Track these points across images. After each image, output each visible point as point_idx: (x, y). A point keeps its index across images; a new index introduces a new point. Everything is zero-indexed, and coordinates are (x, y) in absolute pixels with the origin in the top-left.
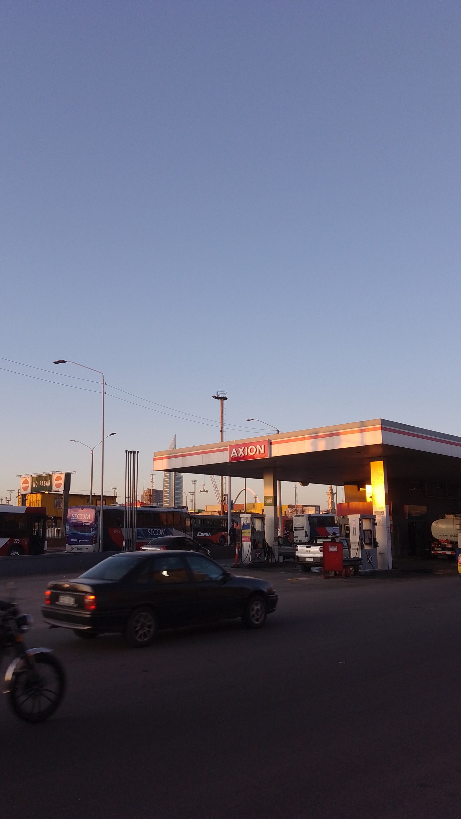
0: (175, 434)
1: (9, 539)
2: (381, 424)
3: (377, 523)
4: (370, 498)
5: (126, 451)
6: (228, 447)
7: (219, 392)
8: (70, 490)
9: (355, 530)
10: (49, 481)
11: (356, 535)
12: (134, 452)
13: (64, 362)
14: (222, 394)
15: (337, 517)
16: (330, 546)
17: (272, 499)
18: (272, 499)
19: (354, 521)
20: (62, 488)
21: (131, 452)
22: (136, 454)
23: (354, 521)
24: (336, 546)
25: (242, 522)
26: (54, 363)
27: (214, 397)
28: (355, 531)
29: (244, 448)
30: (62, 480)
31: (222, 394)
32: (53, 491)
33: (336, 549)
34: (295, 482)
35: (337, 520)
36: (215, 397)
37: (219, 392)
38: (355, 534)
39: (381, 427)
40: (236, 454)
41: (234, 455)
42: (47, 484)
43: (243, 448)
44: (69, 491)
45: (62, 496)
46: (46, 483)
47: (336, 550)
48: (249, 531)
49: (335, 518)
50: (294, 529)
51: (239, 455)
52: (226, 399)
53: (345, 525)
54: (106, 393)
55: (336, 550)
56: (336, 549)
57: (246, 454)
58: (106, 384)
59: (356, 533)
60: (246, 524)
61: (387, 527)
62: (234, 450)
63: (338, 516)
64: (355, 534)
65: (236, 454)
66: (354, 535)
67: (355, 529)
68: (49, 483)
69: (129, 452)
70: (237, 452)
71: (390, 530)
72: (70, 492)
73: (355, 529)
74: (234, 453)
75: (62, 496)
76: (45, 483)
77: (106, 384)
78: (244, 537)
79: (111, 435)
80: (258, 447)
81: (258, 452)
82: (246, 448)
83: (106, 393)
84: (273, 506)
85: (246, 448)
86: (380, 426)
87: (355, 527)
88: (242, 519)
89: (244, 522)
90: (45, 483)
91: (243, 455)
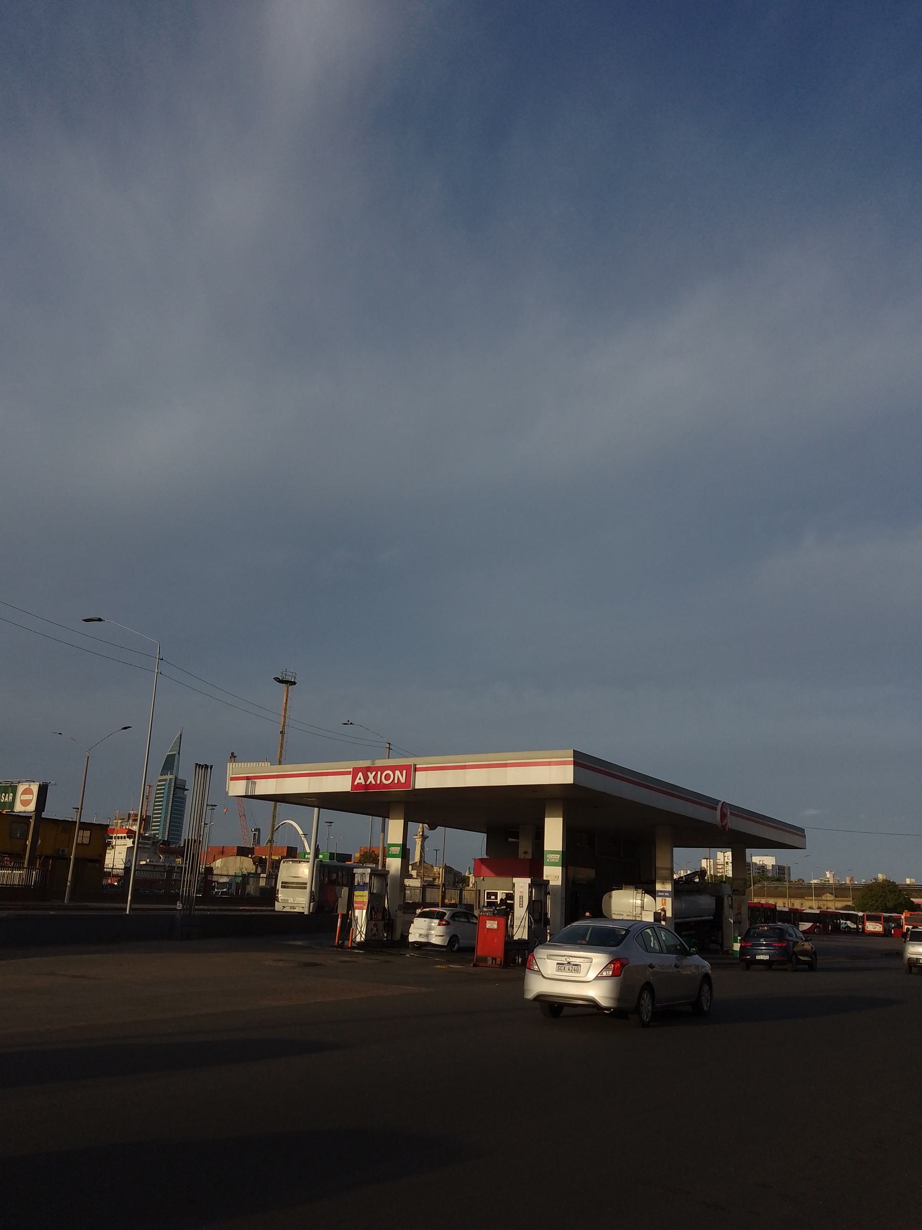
0: (183, 727)
1: (812, 924)
2: (574, 757)
3: (550, 892)
4: (524, 853)
5: (197, 764)
6: (352, 770)
7: (285, 673)
8: (44, 811)
9: (522, 899)
10: (11, 794)
11: (522, 907)
12: (207, 767)
13: (100, 620)
14: (289, 675)
15: (474, 877)
16: (488, 922)
17: (399, 848)
18: (399, 848)
19: (522, 887)
20: (32, 807)
21: (203, 766)
22: (209, 769)
23: (522, 887)
24: (496, 922)
25: (356, 880)
26: (84, 620)
27: (277, 679)
28: (522, 901)
29: (377, 773)
30: (33, 794)
31: (289, 675)
32: (15, 811)
33: (495, 926)
34: (372, 815)
35: (473, 882)
36: (277, 680)
37: (285, 673)
38: (521, 906)
39: (574, 761)
40: (362, 781)
41: (360, 781)
42: (6, 799)
43: (374, 773)
44: (43, 813)
45: (31, 820)
46: (5, 797)
47: (496, 928)
48: (366, 893)
49: (471, 880)
50: (282, 886)
51: (368, 783)
52: (294, 683)
53: (485, 891)
54: (161, 673)
55: (496, 928)
56: (495, 926)
57: (378, 782)
58: (162, 659)
59: (522, 904)
60: (361, 884)
61: (562, 898)
62: (360, 775)
63: (475, 877)
64: (521, 906)
65: (362, 781)
66: (520, 907)
67: (521, 898)
68: (11, 798)
69: (200, 765)
70: (366, 778)
71: (564, 901)
72: (44, 815)
73: (521, 898)
74: (360, 779)
75: (31, 820)
76: (3, 798)
77: (162, 659)
78: (357, 903)
79: (123, 730)
80: (397, 773)
81: (396, 781)
82: (379, 773)
83: (161, 673)
84: (400, 859)
85: (379, 773)
86: (572, 759)
87: (523, 896)
88: (356, 875)
89: (359, 881)
90: (3, 798)
91: (374, 782)
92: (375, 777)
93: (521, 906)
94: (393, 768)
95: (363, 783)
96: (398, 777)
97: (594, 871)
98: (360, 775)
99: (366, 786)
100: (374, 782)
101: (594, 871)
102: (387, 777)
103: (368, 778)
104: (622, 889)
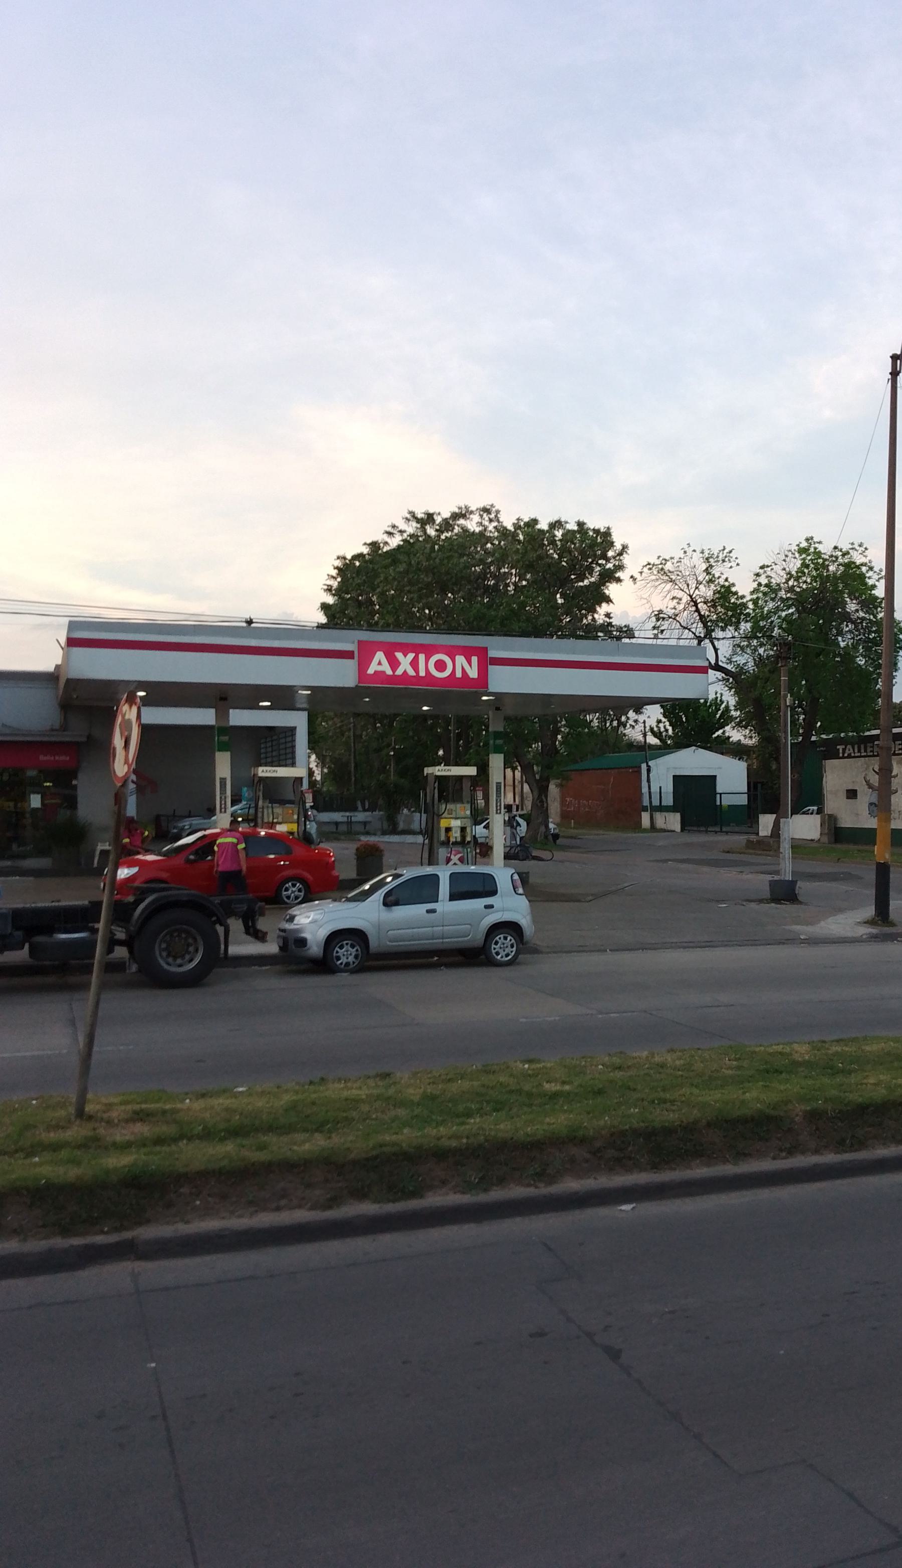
41: (380, 668)
57: (422, 673)
66: (497, 813)
74: (380, 663)
82: (422, 657)
91: (411, 672)
92: (414, 664)
93: (499, 811)
94: (452, 652)
95: (389, 672)
96: (470, 665)
97: (475, 768)
98: (380, 656)
99: (393, 679)
100: (411, 672)
101: (475, 768)
102: (441, 666)
103: (398, 664)
104: (729, 806)
